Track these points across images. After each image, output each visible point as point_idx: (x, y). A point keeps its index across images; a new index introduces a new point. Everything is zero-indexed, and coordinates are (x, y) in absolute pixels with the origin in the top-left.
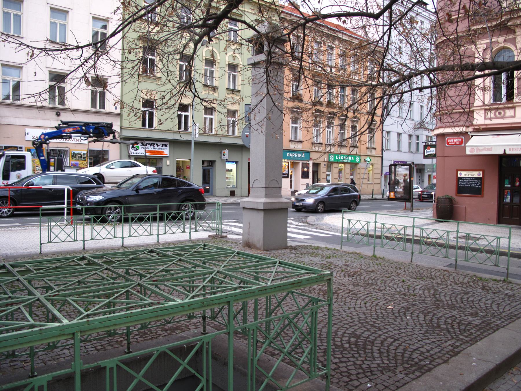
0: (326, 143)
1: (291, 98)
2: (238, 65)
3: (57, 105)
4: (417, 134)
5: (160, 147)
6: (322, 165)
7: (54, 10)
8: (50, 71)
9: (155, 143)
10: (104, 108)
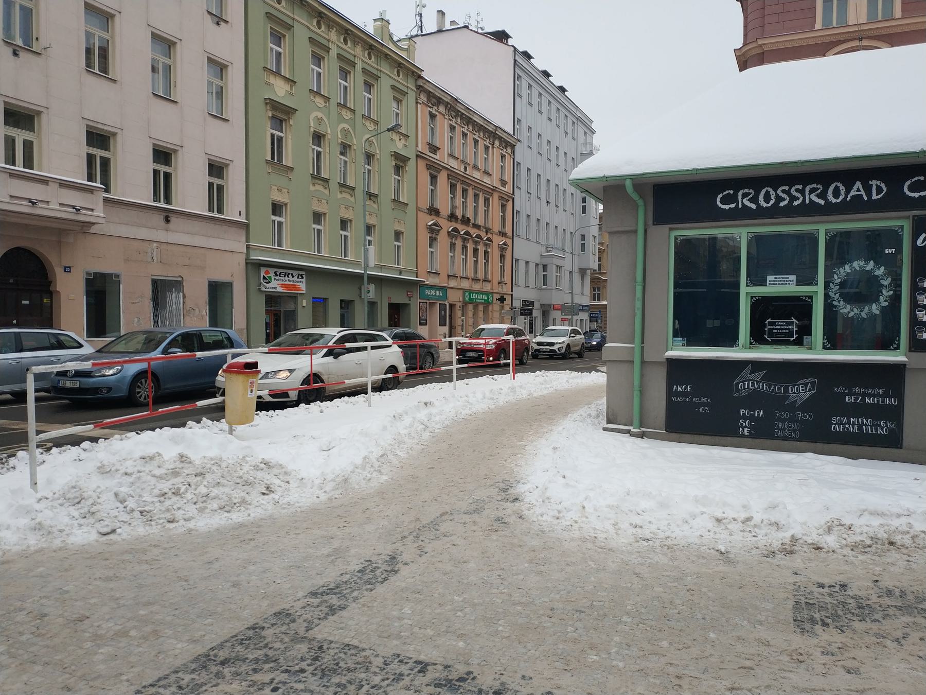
0: (461, 276)
1: (428, 209)
2: (324, 136)
3: (162, 205)
4: (545, 263)
5: (295, 278)
6: (458, 307)
7: (157, 38)
8: (87, 126)
9: (290, 272)
10: (220, 211)
